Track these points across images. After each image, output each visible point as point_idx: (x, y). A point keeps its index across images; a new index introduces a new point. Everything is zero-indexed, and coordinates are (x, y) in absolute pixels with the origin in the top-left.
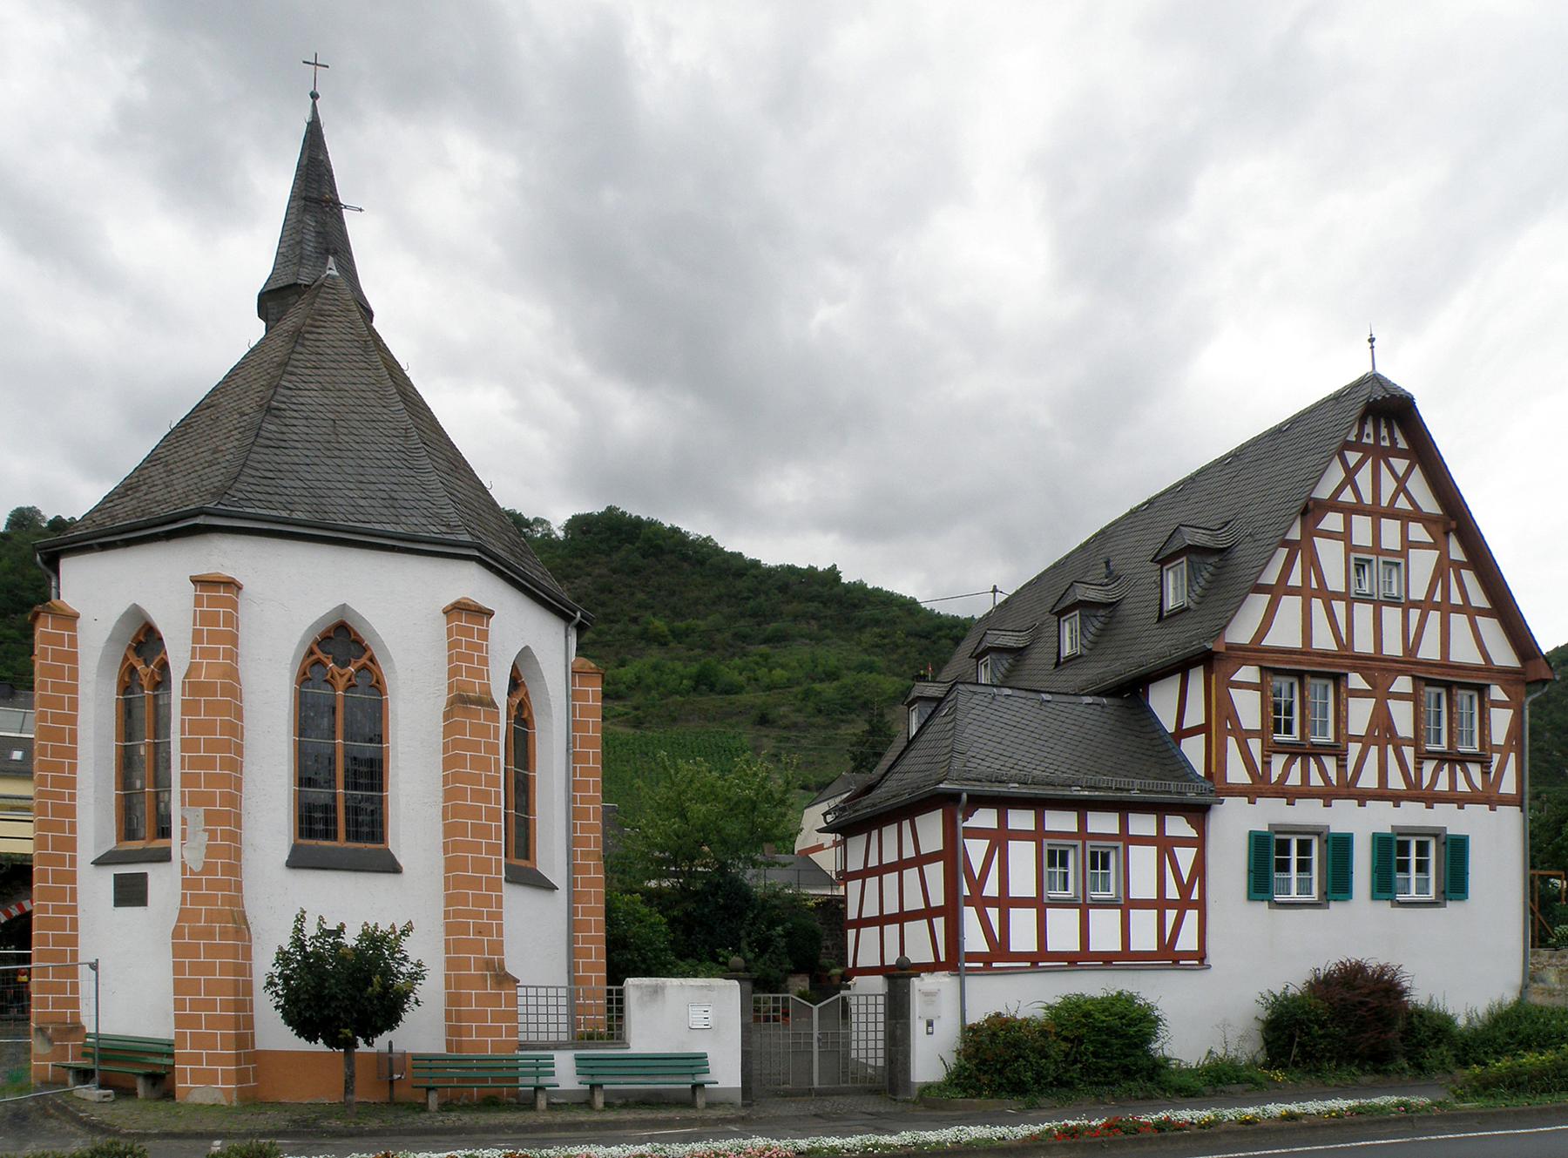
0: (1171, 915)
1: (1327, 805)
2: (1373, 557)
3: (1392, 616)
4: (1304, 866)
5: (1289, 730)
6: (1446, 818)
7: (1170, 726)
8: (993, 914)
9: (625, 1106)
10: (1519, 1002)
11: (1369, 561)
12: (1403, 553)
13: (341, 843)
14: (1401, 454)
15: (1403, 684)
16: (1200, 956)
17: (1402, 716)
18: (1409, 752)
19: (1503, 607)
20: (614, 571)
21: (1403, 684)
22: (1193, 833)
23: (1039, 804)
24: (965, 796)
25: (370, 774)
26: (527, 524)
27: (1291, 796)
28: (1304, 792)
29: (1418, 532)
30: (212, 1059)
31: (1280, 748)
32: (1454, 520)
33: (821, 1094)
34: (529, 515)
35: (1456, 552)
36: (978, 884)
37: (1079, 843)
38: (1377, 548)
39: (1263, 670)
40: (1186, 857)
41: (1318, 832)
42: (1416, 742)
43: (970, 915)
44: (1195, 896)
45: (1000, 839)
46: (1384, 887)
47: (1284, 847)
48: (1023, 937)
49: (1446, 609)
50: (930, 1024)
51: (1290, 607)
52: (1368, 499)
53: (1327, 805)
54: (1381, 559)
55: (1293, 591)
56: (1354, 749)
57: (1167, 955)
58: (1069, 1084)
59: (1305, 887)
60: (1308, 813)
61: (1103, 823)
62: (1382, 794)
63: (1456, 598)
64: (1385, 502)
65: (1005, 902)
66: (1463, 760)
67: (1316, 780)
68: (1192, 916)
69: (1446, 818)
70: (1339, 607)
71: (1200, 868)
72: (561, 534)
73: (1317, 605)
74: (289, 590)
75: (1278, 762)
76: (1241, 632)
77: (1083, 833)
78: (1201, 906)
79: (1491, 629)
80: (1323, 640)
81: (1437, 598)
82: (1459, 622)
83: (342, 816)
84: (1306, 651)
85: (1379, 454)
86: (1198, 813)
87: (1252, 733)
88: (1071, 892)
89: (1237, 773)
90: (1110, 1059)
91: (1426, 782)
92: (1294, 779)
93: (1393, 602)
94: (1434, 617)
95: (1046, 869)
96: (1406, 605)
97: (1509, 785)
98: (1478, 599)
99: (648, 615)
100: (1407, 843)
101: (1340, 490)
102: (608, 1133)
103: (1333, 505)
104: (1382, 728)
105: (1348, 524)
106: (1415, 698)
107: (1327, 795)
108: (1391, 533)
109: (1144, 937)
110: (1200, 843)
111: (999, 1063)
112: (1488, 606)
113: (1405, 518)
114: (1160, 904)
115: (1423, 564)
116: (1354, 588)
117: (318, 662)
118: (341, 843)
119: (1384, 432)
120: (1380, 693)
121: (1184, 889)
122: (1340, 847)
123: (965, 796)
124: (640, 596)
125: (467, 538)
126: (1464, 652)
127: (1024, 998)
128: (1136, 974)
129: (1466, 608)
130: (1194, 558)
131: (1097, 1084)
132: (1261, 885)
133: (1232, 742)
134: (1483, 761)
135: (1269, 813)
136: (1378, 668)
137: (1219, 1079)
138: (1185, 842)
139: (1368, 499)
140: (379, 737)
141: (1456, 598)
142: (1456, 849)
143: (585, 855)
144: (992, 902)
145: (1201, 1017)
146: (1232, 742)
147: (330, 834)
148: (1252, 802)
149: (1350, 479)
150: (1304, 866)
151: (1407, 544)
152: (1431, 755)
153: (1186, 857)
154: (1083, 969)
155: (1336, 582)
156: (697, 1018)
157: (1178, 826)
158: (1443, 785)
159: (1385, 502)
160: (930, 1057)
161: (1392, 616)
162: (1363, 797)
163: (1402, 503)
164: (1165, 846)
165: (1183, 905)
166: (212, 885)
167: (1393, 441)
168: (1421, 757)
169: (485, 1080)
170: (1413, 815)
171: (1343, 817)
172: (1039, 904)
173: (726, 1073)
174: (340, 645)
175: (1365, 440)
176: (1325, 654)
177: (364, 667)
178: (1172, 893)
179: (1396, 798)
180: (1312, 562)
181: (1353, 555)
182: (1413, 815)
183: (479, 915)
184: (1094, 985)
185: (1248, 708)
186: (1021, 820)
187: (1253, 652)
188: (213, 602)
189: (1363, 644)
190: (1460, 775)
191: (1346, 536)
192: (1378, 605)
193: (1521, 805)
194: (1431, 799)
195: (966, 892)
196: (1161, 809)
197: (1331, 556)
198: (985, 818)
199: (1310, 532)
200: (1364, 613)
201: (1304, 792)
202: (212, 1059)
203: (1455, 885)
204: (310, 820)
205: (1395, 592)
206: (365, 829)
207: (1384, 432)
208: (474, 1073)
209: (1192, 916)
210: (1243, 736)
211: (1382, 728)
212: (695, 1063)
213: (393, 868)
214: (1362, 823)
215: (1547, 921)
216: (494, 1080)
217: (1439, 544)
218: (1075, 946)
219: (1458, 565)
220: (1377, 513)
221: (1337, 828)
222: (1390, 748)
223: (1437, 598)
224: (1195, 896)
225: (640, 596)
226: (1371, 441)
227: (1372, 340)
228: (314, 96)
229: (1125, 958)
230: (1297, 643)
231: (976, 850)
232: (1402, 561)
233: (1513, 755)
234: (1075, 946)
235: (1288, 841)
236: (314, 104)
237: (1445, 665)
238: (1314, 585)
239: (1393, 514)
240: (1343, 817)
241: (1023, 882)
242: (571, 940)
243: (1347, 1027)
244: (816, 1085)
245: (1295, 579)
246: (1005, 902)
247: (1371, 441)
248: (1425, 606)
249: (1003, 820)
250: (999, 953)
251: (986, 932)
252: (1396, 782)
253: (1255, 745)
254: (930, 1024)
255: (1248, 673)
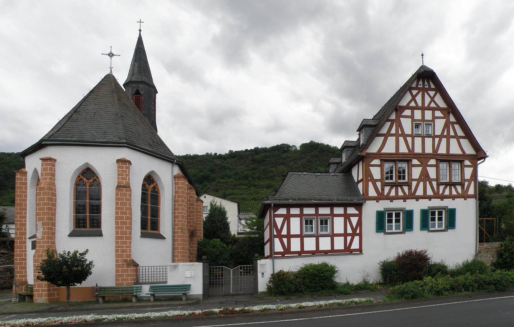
0: (349, 238)
1: (405, 201)
2: (422, 123)
3: (429, 141)
4: (440, 219)
5: (404, 179)
6: (449, 203)
7: (356, 181)
8: (285, 240)
9: (165, 300)
10: (474, 261)
11: (421, 124)
12: (433, 120)
13: (88, 229)
14: (432, 90)
15: (433, 162)
16: (360, 251)
17: (432, 172)
18: (434, 183)
19: (469, 135)
20: (312, 157)
21: (433, 162)
22: (357, 212)
23: (301, 206)
24: (272, 205)
25: (97, 209)
26: (290, 147)
27: (392, 199)
28: (397, 197)
29: (438, 114)
30: (42, 291)
31: (387, 184)
32: (451, 109)
33: (233, 295)
34: (291, 145)
35: (452, 119)
36: (279, 231)
37: (315, 217)
38: (423, 119)
39: (381, 160)
40: (354, 220)
41: (402, 210)
42: (437, 180)
43: (277, 241)
44: (358, 232)
45: (287, 218)
46: (424, 226)
47: (433, 214)
48: (295, 245)
49: (449, 137)
50: (263, 274)
51: (391, 140)
52: (420, 104)
53: (405, 201)
54: (425, 123)
55: (392, 135)
56: (414, 184)
57: (348, 250)
58: (302, 292)
59: (440, 225)
60: (398, 204)
61: (324, 211)
62: (425, 197)
63: (452, 133)
64: (426, 105)
65: (289, 236)
66: (455, 184)
67: (400, 193)
68: (357, 238)
69: (449, 203)
70: (409, 139)
71: (359, 223)
72: (299, 149)
73: (401, 139)
74: (103, 161)
75: (387, 189)
76: (374, 148)
77: (317, 214)
78: (360, 235)
79: (465, 143)
80: (403, 149)
81: (445, 134)
82: (453, 142)
83: (87, 221)
84: (397, 153)
85: (424, 90)
86: (359, 206)
87: (377, 180)
88: (314, 232)
89: (372, 193)
90: (316, 284)
91: (441, 192)
92: (393, 193)
93: (429, 136)
94: (444, 140)
95: (304, 225)
96: (434, 137)
97: (471, 192)
98: (460, 133)
99: (320, 167)
100: (435, 212)
101: (410, 102)
102: (142, 309)
103: (407, 107)
104: (425, 177)
105: (413, 113)
106: (437, 166)
107: (405, 198)
108: (428, 115)
109: (339, 244)
110: (360, 216)
111: (284, 286)
112: (464, 135)
113: (433, 110)
114: (345, 235)
115: (440, 124)
116: (414, 132)
117: (81, 179)
118: (88, 229)
119: (426, 83)
120: (424, 165)
121: (354, 230)
122: (409, 214)
123: (272, 205)
124: (318, 163)
125: (125, 141)
126: (455, 150)
127: (291, 266)
128: (336, 256)
129: (456, 136)
130: (367, 128)
131: (312, 291)
132: (380, 227)
133: (370, 184)
134: (462, 184)
135: (383, 205)
136: (423, 158)
137: (363, 288)
138: (354, 215)
139: (420, 104)
140: (99, 199)
141: (452, 133)
142: (452, 213)
143: (178, 229)
144: (284, 236)
145: (350, 271)
146: (370, 184)
147: (85, 227)
148: (378, 202)
149: (414, 98)
150: (440, 219)
151: (434, 118)
152: (442, 184)
153: (354, 220)
154: (317, 256)
155: (408, 130)
156: (188, 274)
157: (351, 210)
158: (447, 192)
159: (426, 105)
160: (263, 283)
161: (429, 141)
162: (418, 198)
163: (433, 105)
164: (347, 217)
165: (353, 235)
166: (44, 242)
167: (429, 86)
168: (438, 185)
169: (123, 294)
170: (436, 203)
171: (410, 205)
172: (301, 237)
173: (197, 289)
174: (87, 176)
175: (419, 86)
176: (404, 154)
177: (154, 187)
178: (349, 231)
179: (430, 198)
180: (400, 126)
181: (414, 123)
182: (436, 203)
183: (123, 247)
184: (317, 261)
185: (376, 173)
186: (295, 211)
187: (378, 155)
188: (46, 165)
189: (418, 150)
190: (453, 189)
191: (412, 117)
192: (423, 138)
193: (476, 198)
194: (442, 197)
195: (275, 233)
196: (345, 206)
197: (407, 125)
198: (283, 211)
199: (399, 116)
200: (418, 141)
201: (397, 197)
202: (42, 291)
203: (451, 224)
204: (79, 223)
205: (430, 133)
206: (95, 225)
207: (426, 83)
208: (120, 292)
209: (357, 238)
210: (374, 182)
211: (425, 177)
212: (187, 287)
213: (162, 238)
214: (417, 207)
215: (485, 234)
216: (126, 294)
217: (446, 116)
218: (314, 249)
219: (453, 123)
220: (423, 109)
221: (408, 208)
222: (428, 182)
223: (445, 134)
224: (358, 232)
225: (318, 163)
226: (421, 86)
227: (422, 55)
228: (140, 31)
229: (333, 252)
230: (394, 151)
231: (279, 221)
232: (432, 123)
233: (473, 182)
234: (314, 249)
235: (392, 213)
236: (140, 33)
237: (448, 155)
238: (400, 133)
239: (429, 108)
240: (410, 205)
241: (295, 229)
242: (173, 253)
243: (409, 269)
244: (231, 292)
245: (393, 131)
246: (289, 236)
247: (421, 86)
248: (441, 137)
249: (288, 211)
250: (287, 252)
251: (295, 244)
252: (430, 192)
253: (379, 184)
254: (263, 274)
255: (376, 162)
